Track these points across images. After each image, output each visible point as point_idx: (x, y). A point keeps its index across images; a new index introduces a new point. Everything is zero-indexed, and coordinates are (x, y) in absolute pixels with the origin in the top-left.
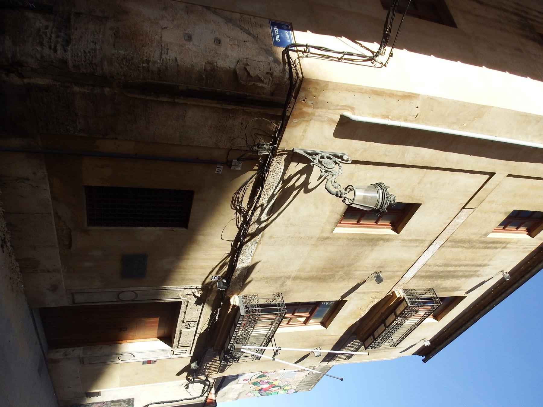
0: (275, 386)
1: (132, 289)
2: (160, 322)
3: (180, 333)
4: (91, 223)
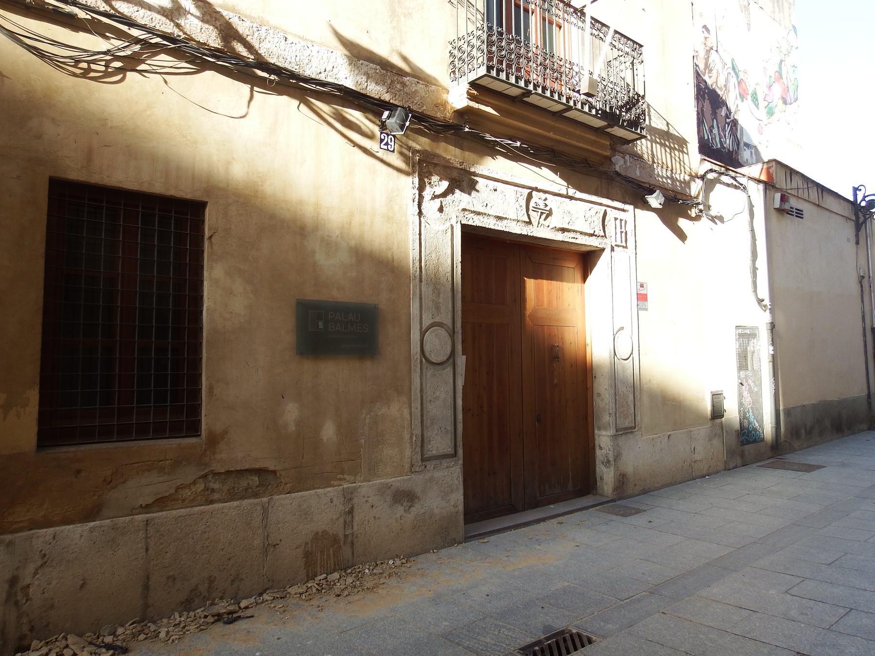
0: (780, 72)
1: (415, 335)
2: (536, 276)
3: (563, 230)
4: (194, 429)
